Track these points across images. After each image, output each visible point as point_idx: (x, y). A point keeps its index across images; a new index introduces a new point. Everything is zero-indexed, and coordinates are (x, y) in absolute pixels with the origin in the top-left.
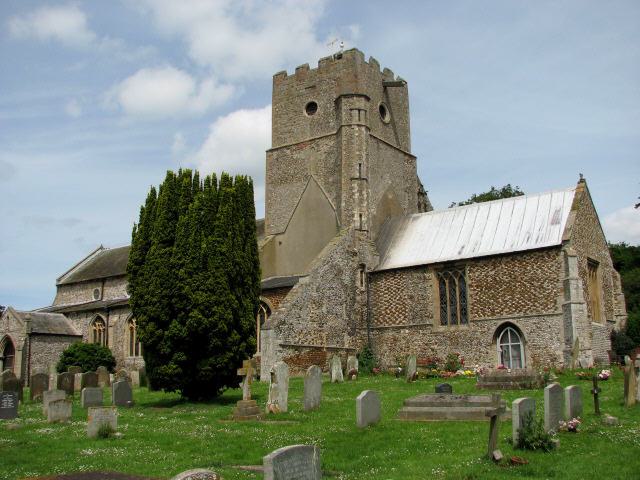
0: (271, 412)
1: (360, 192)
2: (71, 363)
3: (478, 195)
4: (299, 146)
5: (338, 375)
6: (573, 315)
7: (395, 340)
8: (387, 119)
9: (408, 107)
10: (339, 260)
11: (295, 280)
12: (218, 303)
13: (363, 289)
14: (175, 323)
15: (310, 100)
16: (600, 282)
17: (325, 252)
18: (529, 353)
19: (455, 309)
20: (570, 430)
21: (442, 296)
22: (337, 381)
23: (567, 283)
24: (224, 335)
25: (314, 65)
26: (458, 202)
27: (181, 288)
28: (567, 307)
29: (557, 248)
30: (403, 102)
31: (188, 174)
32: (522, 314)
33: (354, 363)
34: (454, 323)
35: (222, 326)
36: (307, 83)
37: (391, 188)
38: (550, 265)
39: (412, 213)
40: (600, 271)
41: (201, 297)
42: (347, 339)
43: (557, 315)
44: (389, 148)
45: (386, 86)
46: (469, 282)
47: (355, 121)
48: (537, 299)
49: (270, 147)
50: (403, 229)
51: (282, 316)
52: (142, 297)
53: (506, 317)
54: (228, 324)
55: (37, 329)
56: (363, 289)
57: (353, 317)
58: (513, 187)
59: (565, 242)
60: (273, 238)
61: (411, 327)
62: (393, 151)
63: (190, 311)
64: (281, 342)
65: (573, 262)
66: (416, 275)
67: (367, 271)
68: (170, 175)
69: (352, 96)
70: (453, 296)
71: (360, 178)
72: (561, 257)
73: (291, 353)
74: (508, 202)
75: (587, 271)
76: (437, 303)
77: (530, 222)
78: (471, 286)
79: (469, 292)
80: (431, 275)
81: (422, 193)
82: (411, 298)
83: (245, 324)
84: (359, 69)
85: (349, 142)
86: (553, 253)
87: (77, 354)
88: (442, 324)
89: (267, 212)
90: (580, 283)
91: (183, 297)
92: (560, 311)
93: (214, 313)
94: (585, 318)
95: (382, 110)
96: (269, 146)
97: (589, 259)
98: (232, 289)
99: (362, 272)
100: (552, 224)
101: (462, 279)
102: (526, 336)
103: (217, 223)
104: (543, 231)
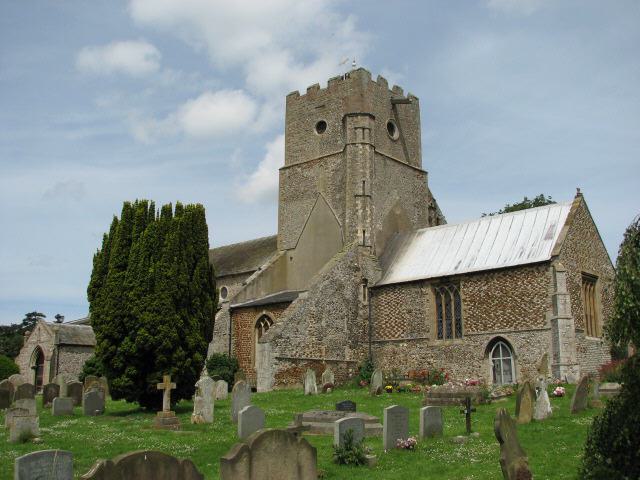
0: (195, 423)
1: (364, 208)
2: (91, 372)
3: (511, 205)
4: (309, 164)
5: (312, 388)
6: (560, 330)
7: (395, 353)
8: (396, 135)
9: (419, 123)
10: (340, 276)
11: (295, 295)
12: (163, 323)
13: (366, 303)
14: (127, 339)
15: (320, 119)
16: (599, 296)
17: (327, 267)
18: (519, 367)
19: (450, 325)
20: (408, 448)
21: (439, 306)
22: (310, 394)
23: (555, 298)
24: (169, 352)
25: (324, 85)
26: (488, 214)
27: (131, 309)
28: (554, 322)
29: (546, 263)
30: (414, 119)
31: (144, 204)
32: (512, 329)
33: (329, 377)
34: (449, 336)
35: (166, 343)
36: (317, 103)
37: (399, 204)
38: (539, 281)
39: (418, 229)
40: (599, 285)
41: (147, 317)
42: (348, 354)
43: (546, 330)
44: (397, 164)
45: (394, 104)
46: (463, 297)
47: (359, 139)
48: (531, 315)
49: (283, 165)
50: (408, 244)
51: (278, 331)
52: (98, 316)
53: (498, 332)
54: (173, 342)
55: (65, 341)
56: (366, 303)
57: (354, 329)
58: (546, 198)
59: (554, 257)
60: (285, 254)
61: (409, 341)
62: (401, 167)
63: (138, 329)
64: (277, 355)
65: (561, 278)
66: (414, 290)
67: (369, 285)
68: (127, 206)
69: (356, 115)
70: (448, 311)
71: (364, 195)
72: (550, 273)
73: (287, 365)
74: (542, 211)
75: (581, 285)
76: (434, 318)
77: (527, 238)
78: (465, 301)
79: (463, 306)
80: (428, 290)
81: (433, 208)
82: (410, 312)
83: (191, 341)
84: (366, 88)
85: (354, 160)
86: (542, 269)
87: (97, 364)
88: (439, 338)
89: (281, 222)
90: (568, 298)
91: (132, 317)
92: (549, 326)
93: (159, 332)
94: (572, 333)
95: (391, 127)
96: (282, 164)
97: (583, 273)
98: (177, 309)
99: (364, 287)
100: (545, 239)
101: (457, 294)
102: (516, 349)
103: (164, 249)
104: (536, 247)
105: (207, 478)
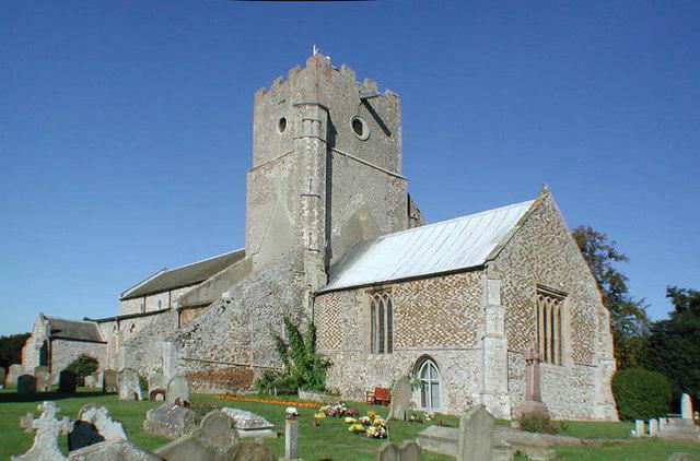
1: (311, 209)
34: (382, 351)
47: (307, 132)
48: (463, 333)
80: (364, 298)
105: (280, 459)
